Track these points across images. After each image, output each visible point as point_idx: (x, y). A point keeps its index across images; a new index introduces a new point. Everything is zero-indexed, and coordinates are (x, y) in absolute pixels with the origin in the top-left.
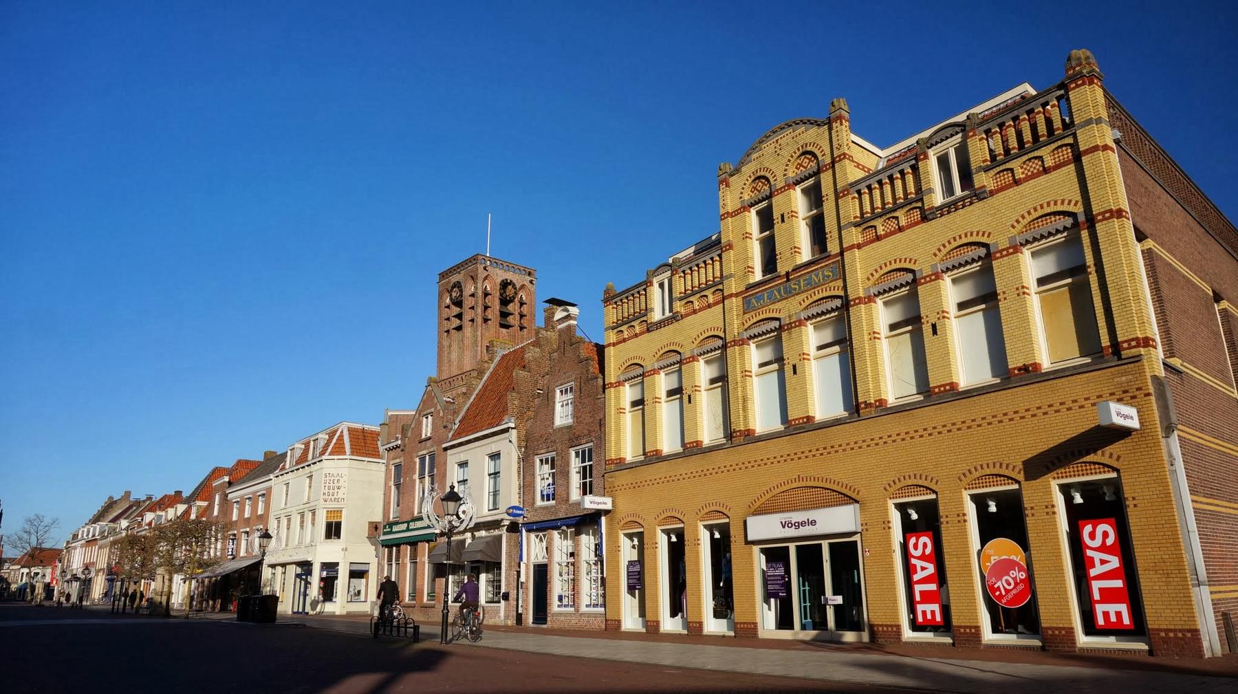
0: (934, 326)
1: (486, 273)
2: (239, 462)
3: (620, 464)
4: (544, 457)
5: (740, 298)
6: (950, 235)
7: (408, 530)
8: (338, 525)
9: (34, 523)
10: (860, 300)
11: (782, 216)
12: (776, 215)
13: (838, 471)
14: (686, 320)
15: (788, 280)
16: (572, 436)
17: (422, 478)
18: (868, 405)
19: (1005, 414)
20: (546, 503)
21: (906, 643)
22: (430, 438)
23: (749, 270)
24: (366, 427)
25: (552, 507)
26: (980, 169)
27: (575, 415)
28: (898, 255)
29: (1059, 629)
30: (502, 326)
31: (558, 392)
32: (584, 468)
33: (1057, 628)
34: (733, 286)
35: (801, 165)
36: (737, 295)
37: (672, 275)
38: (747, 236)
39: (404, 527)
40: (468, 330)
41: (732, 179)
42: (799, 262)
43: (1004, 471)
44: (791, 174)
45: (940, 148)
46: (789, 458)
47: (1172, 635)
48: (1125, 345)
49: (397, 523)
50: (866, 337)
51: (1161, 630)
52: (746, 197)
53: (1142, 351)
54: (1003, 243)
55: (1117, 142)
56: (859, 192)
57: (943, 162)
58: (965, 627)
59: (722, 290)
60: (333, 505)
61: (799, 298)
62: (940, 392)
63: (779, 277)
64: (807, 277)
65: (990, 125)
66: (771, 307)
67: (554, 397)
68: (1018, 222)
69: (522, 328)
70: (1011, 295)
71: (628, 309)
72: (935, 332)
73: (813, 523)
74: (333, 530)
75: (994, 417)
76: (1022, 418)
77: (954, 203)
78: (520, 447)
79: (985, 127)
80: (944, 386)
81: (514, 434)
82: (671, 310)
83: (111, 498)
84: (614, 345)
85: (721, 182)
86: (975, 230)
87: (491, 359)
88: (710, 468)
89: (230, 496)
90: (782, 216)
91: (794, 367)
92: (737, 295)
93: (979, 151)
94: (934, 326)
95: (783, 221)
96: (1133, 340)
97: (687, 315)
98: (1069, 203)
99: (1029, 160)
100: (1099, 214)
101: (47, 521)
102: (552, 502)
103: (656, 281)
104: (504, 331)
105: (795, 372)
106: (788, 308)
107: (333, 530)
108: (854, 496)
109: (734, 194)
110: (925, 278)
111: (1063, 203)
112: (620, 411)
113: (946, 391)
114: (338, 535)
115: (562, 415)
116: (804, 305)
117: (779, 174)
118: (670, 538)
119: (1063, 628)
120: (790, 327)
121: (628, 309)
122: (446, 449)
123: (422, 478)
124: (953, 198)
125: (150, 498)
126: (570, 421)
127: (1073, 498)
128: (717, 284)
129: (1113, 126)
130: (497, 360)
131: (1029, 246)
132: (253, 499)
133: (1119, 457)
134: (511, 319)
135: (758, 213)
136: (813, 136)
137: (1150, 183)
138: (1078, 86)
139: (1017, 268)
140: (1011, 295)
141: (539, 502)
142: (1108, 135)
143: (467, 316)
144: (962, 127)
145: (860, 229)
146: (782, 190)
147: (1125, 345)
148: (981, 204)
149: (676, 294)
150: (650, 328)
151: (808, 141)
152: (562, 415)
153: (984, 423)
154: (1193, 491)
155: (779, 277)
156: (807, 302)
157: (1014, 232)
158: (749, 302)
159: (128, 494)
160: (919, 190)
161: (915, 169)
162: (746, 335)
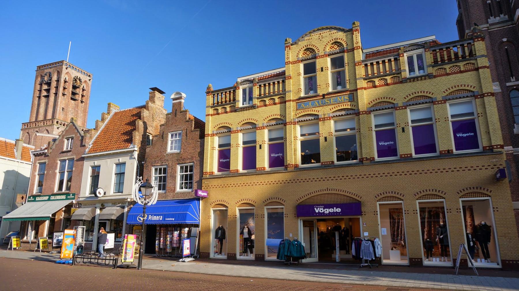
0: (260, 146)
1: (67, 71)
5: (295, 103)
6: (413, 91)
10: (291, 123)
14: (260, 109)
15: (324, 98)
18: (367, 159)
19: (328, 180)
20: (184, 190)
21: (384, 265)
23: (299, 90)
24: (7, 141)
26: (361, 78)
30: (72, 99)
32: (160, 177)
35: (333, 47)
36: (293, 101)
38: (299, 74)
41: (291, 47)
43: (437, 193)
44: (328, 50)
47: (511, 262)
50: (293, 139)
51: (507, 260)
52: (300, 56)
54: (439, 98)
56: (260, 86)
57: (244, 91)
58: (415, 259)
61: (331, 107)
62: (405, 157)
64: (335, 98)
66: (314, 109)
67: (167, 137)
68: (407, 96)
69: (82, 102)
72: (260, 148)
76: (372, 177)
84: (211, 115)
85: (287, 47)
86: (426, 91)
92: (293, 101)
93: (256, 92)
94: (260, 146)
96: (499, 145)
97: (261, 107)
99: (453, 66)
100: (486, 93)
104: (73, 102)
106: (322, 111)
109: (294, 53)
110: (438, 101)
116: (333, 110)
120: (324, 119)
130: (112, 114)
131: (268, 127)
134: (77, 97)
135: (305, 65)
136: (340, 36)
138: (478, 41)
139: (237, 138)
144: (251, 81)
145: (366, 81)
147: (495, 147)
148: (429, 80)
150: (235, 110)
151: (338, 37)
155: (318, 96)
156: (334, 110)
157: (445, 94)
158: (300, 105)
160: (234, 100)
161: (234, 91)
162: (297, 120)
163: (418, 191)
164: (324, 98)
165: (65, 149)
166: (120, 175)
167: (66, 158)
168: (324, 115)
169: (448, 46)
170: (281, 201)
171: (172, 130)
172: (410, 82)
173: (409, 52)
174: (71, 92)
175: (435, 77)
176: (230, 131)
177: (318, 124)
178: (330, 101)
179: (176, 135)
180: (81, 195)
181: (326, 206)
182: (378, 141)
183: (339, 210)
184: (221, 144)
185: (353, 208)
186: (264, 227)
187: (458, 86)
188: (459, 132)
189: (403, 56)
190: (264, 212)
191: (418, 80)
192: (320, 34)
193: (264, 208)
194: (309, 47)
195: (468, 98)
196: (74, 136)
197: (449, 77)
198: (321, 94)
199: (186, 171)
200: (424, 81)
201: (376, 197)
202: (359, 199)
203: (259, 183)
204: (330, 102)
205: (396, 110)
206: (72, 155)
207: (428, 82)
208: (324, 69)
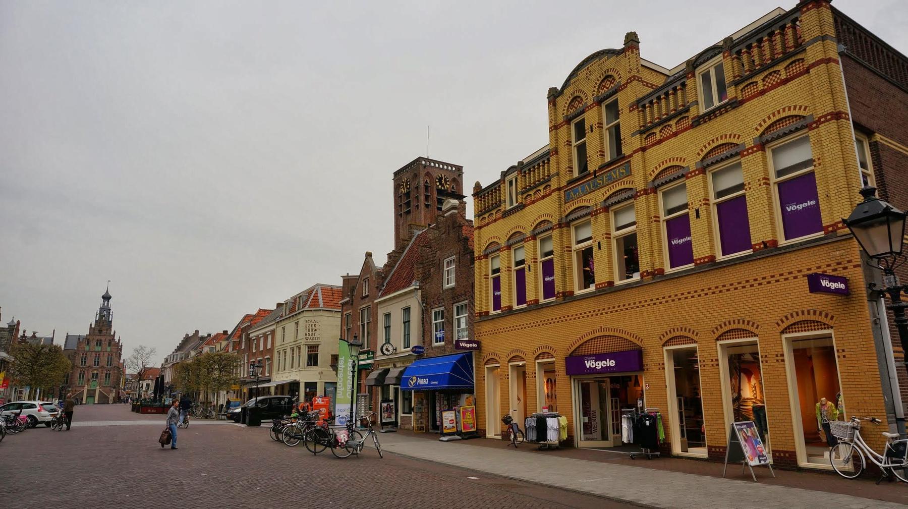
2: (260, 310)
4: (437, 310)
6: (710, 138)
8: (316, 356)
9: (139, 351)
10: (479, 258)
12: (587, 126)
16: (455, 295)
22: (367, 296)
23: (571, 170)
28: (671, 155)
33: (783, 452)
34: (554, 184)
55: (841, 54)
57: (706, 77)
60: (311, 342)
61: (602, 191)
63: (589, 174)
66: (584, 198)
74: (313, 360)
77: (713, 112)
83: (187, 335)
87: (410, 238)
88: (642, 300)
89: (251, 336)
91: (599, 243)
95: (592, 131)
97: (529, 204)
98: (800, 108)
99: (770, 74)
101: (148, 350)
102: (443, 343)
105: (600, 248)
107: (313, 360)
111: (795, 109)
113: (704, 262)
114: (316, 364)
115: (449, 282)
117: (589, 94)
121: (489, 201)
122: (378, 304)
124: (713, 108)
125: (209, 335)
132: (265, 336)
133: (832, 318)
137: (883, 86)
146: (590, 107)
148: (732, 113)
151: (609, 67)
152: (449, 282)
153: (732, 288)
155: (589, 174)
158: (569, 194)
159: (197, 332)
163: (717, 323)
164: (595, 177)
169: (749, 42)
170: (749, 328)
172: (705, 122)
175: (742, 103)
181: (599, 357)
182: (670, 239)
183: (612, 363)
185: (632, 359)
187: (779, 112)
188: (790, 203)
191: (716, 117)
197: (764, 97)
200: (726, 115)
202: (639, 343)
205: (688, 178)
207: (731, 116)
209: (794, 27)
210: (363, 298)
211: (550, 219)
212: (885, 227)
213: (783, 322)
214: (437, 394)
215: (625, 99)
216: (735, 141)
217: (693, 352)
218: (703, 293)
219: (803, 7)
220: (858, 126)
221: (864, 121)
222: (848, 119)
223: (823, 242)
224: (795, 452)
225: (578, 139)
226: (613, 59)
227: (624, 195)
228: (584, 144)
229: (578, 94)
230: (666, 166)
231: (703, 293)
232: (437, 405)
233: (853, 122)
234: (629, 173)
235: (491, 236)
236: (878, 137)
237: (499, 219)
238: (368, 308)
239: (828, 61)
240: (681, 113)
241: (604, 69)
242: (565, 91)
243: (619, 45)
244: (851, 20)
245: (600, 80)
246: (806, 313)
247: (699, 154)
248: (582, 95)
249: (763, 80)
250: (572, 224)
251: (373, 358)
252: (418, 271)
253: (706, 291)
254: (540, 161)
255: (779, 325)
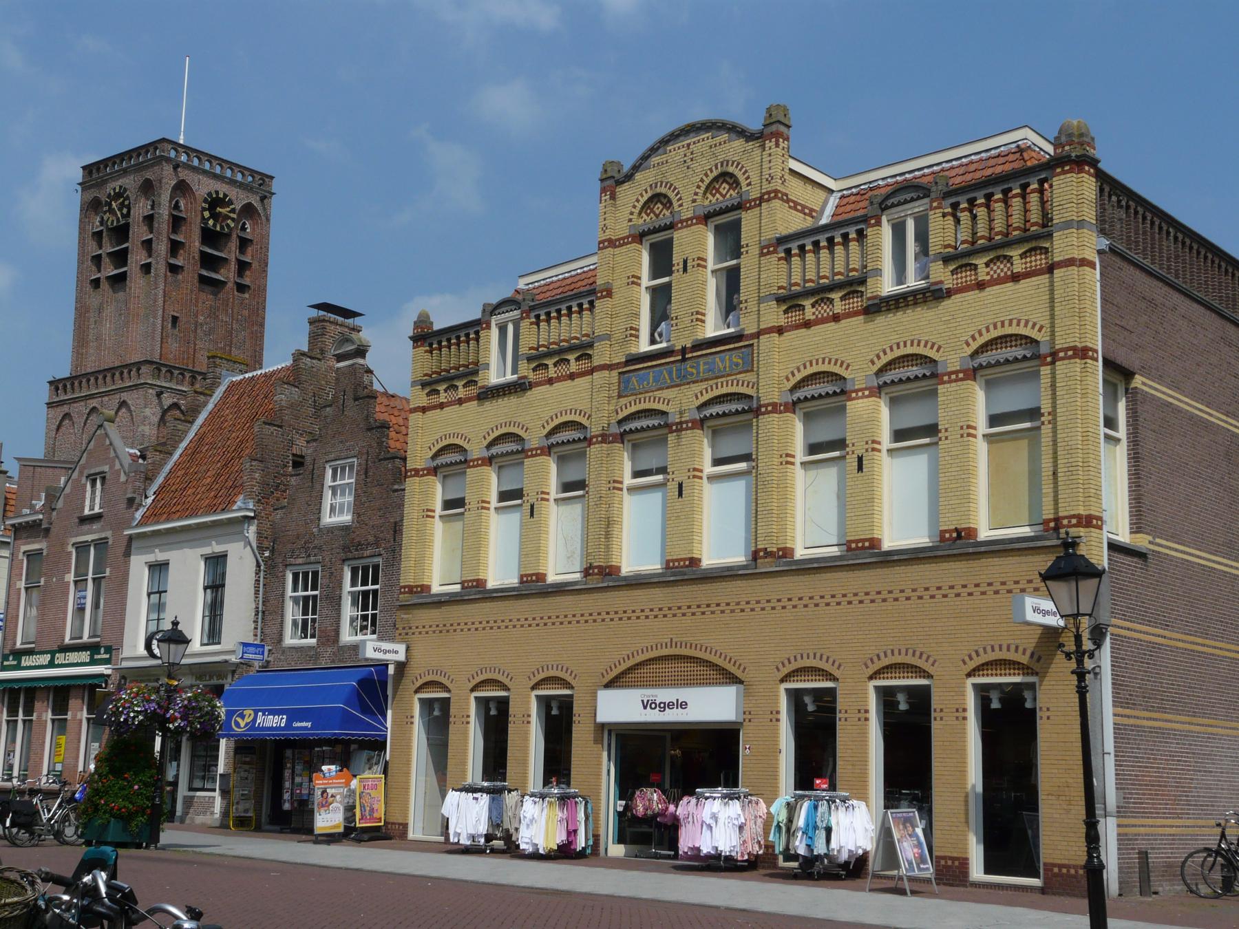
0: (860, 459)
3: (421, 598)
6: (894, 338)
7: (51, 665)
10: (417, 472)
11: (685, 262)
12: (677, 259)
13: (715, 638)
16: (348, 543)
17: (80, 583)
22: (96, 518)
23: (634, 333)
25: (310, 648)
27: (358, 509)
29: (953, 859)
31: (329, 472)
32: (305, 622)
33: (951, 858)
34: (602, 354)
37: (522, 318)
39: (45, 659)
40: (136, 282)
42: (700, 336)
45: (897, 213)
46: (661, 613)
47: (1064, 871)
48: (1065, 522)
49: (30, 652)
53: (1082, 531)
59: (589, 356)
61: (696, 388)
62: (857, 548)
64: (710, 359)
65: (959, 199)
66: (658, 394)
67: (323, 476)
70: (954, 434)
71: (451, 358)
73: (683, 705)
75: (914, 590)
78: (261, 549)
79: (953, 200)
80: (863, 541)
81: (251, 532)
82: (514, 371)
83: (1098, 161)
86: (924, 339)
90: (685, 262)
95: (685, 270)
96: (1073, 516)
97: (539, 384)
100: (1061, 350)
103: (494, 320)
108: (738, 673)
112: (428, 513)
113: (863, 548)
115: (336, 508)
117: (687, 197)
118: (488, 710)
119: (957, 859)
121: (451, 358)
123: (80, 583)
126: (346, 518)
127: (990, 700)
128: (583, 349)
129: (1102, 232)
140: (954, 434)
141: (290, 640)
142: (1090, 244)
143: (137, 257)
146: (687, 223)
149: (523, 350)
152: (336, 508)
154: (1115, 704)
158: (628, 381)
161: (861, 234)
164: (684, 360)
165: (87, 512)
166: (216, 586)
167: (89, 538)
168: (681, 413)
171: (332, 456)
173: (893, 210)
174: (197, 256)
175: (949, 293)
176: (934, 375)
177: (666, 440)
178: (697, 368)
179: (343, 469)
180: (126, 652)
184: (898, 427)
186: (42, 755)
189: (879, 223)
190: (528, 709)
192: (689, 145)
193: (468, 699)
194: (658, 190)
195: (924, 383)
196: (106, 468)
198: (678, 347)
199: (365, 583)
201: (866, 665)
203: (546, 620)
204: (698, 373)
206: (102, 530)
208: (689, 264)
209: (1041, 191)
210: (84, 520)
211: (584, 421)
212: (1074, 584)
213: (971, 659)
214: (289, 753)
215: (755, 228)
216: (932, 354)
217: (832, 692)
218: (855, 600)
219: (1057, 166)
220: (1109, 364)
221: (1122, 358)
222: (1097, 360)
223: (1031, 544)
224: (967, 859)
225: (655, 274)
226: (739, 144)
227: (734, 407)
228: (668, 286)
229: (663, 190)
230: (815, 369)
231: (855, 600)
232: (287, 773)
233: (1105, 359)
234: (749, 366)
235: (450, 430)
236: (1138, 381)
237: (469, 399)
238: (101, 544)
239: (1084, 262)
240: (853, 285)
241: (721, 158)
242: (638, 176)
243: (755, 124)
244: (128, 574)
245: (711, 176)
246: (1004, 648)
247: (873, 362)
248: (671, 195)
249: (987, 265)
250: (627, 438)
251: (107, 661)
252: (253, 476)
253: (861, 596)
254: (553, 309)
255: (965, 663)
